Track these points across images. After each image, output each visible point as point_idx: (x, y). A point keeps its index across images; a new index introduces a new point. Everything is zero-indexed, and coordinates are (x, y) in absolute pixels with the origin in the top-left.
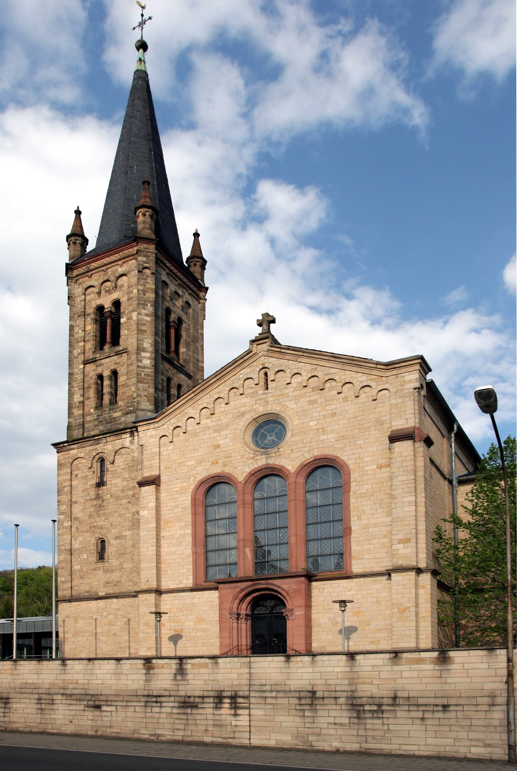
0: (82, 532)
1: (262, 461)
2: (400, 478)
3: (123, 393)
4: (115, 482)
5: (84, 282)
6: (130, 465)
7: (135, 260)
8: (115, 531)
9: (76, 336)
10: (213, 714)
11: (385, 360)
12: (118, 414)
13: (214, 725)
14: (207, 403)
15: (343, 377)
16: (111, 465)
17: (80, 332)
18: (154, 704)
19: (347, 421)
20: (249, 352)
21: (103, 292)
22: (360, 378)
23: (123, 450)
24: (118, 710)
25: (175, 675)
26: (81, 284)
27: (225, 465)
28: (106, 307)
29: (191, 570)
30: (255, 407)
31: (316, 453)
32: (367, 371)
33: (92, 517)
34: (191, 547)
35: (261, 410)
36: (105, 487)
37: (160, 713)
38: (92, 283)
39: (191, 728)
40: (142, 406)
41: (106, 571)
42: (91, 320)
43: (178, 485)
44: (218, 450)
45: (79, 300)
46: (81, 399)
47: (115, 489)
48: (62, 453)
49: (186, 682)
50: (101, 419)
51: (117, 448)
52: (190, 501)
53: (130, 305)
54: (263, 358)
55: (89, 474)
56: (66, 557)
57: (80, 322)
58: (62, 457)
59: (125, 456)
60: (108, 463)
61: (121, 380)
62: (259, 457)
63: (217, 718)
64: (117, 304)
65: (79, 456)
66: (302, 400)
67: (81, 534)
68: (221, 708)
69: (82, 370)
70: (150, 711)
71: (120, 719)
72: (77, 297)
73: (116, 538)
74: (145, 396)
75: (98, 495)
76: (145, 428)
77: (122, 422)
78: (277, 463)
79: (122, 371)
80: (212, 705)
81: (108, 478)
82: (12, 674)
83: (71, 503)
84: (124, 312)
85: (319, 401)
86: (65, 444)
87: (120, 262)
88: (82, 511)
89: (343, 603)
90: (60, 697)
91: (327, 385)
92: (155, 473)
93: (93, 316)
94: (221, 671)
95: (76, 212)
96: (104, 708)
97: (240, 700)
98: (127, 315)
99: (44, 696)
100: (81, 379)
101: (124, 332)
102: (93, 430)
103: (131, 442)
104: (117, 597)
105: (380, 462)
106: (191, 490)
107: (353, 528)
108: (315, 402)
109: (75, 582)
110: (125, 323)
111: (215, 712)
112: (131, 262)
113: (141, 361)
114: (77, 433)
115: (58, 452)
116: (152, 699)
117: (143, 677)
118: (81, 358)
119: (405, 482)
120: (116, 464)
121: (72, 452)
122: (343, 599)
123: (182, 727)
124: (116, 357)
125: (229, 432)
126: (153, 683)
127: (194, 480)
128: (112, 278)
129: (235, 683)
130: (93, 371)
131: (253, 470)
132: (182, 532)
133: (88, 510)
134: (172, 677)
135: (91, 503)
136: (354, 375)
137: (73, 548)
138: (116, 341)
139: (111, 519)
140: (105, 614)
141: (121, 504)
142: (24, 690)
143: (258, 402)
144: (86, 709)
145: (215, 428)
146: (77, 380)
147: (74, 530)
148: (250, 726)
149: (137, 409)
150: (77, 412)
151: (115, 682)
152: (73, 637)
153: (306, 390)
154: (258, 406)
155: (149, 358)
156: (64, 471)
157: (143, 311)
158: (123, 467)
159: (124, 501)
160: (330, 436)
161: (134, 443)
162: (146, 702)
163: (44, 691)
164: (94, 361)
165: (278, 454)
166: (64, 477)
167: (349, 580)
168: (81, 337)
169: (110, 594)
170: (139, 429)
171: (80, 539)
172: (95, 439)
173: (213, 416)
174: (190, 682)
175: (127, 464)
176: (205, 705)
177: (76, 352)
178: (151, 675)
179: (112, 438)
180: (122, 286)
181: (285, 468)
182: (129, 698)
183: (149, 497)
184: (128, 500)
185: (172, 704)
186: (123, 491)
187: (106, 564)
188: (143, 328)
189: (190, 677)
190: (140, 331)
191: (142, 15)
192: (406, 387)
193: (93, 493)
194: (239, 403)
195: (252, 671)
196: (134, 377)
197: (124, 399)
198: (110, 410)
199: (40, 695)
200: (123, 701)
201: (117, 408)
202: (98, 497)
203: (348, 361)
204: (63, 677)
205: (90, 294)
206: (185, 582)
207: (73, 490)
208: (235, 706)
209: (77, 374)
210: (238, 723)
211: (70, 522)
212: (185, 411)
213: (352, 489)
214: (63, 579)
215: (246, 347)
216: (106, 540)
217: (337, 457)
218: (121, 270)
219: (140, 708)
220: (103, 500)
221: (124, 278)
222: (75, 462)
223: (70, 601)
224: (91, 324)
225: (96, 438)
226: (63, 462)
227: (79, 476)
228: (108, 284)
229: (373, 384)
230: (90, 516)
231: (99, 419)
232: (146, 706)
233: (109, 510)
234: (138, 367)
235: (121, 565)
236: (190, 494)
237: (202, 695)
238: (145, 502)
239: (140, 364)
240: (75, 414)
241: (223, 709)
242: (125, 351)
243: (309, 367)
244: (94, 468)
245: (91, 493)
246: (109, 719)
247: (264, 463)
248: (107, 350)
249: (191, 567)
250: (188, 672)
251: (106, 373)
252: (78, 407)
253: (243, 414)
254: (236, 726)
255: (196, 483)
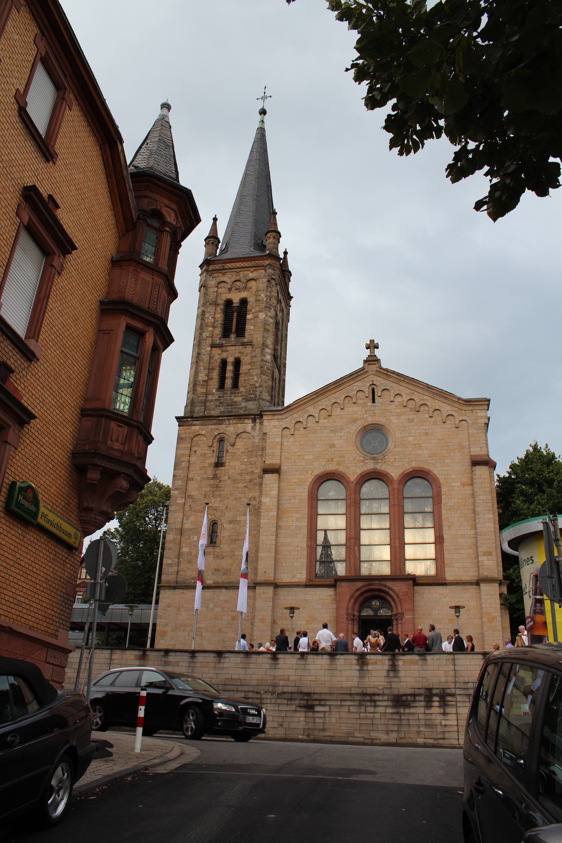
0: (195, 511)
1: (370, 466)
2: (481, 497)
3: (245, 380)
4: (234, 465)
5: (218, 277)
6: (250, 449)
7: (264, 271)
8: (229, 515)
9: (206, 321)
10: (425, 713)
11: (465, 397)
12: (239, 399)
13: (426, 725)
14: (326, 405)
15: (434, 405)
16: (231, 447)
17: (210, 318)
18: (368, 704)
19: (437, 441)
20: (362, 369)
21: (233, 289)
22: (446, 408)
23: (244, 434)
24: (332, 710)
25: (388, 671)
26: (215, 277)
27: (339, 464)
28: (234, 302)
29: (305, 565)
30: (365, 416)
31: (414, 465)
32: (451, 403)
33: (207, 496)
34: (305, 540)
35: (370, 420)
36: (223, 468)
37: (374, 713)
38: (225, 279)
39: (404, 729)
40: (263, 397)
41: (216, 557)
42: (221, 309)
43: (297, 477)
44: (333, 449)
45: (212, 291)
46: (206, 378)
47: (233, 471)
48: (184, 427)
49: (398, 680)
50: (222, 401)
51: (239, 432)
52: (307, 494)
53: (257, 306)
54: (372, 376)
55: (209, 452)
56: (175, 536)
57: (211, 309)
58: (183, 431)
59: (245, 440)
60: (228, 444)
61: (244, 368)
62: (368, 461)
63: (428, 717)
64: (244, 302)
65: (200, 432)
66: (402, 417)
67: (194, 513)
68: (431, 707)
69: (209, 352)
70: (363, 711)
71: (334, 720)
72: (210, 287)
73: (230, 522)
74: (266, 387)
75: (215, 475)
76: (270, 417)
77: (243, 408)
78: (383, 469)
79: (245, 360)
80: (423, 704)
81: (227, 459)
82: (215, 668)
83: (188, 479)
84: (251, 310)
85: (416, 420)
86: (189, 419)
87: (252, 269)
88: (198, 489)
89: (457, 608)
90: (269, 696)
91: (422, 409)
92: (276, 461)
93: (222, 307)
94: (430, 668)
95: (213, 219)
96: (317, 708)
97: (449, 698)
98: (253, 313)
99: (251, 695)
100: (207, 360)
101: (249, 327)
102: (214, 410)
103: (253, 428)
104: (226, 588)
105: (463, 480)
106: (308, 483)
107: (445, 537)
108: (413, 420)
109: (182, 566)
110: (251, 319)
111: (427, 712)
112: (260, 271)
113: (265, 356)
114: (199, 411)
115: (179, 426)
116: (368, 698)
117: (357, 674)
118: (209, 341)
119: (485, 501)
120: (236, 447)
121: (193, 428)
122: (292, 606)
123: (395, 728)
124: (240, 347)
125: (343, 434)
126: (367, 680)
127: (311, 474)
128: (243, 280)
129: (443, 680)
130: (218, 355)
131: (364, 472)
132: (298, 524)
133: (204, 489)
134: (384, 673)
135: (208, 482)
136: (441, 404)
137: (183, 527)
138: (241, 332)
139: (226, 501)
140: (211, 606)
141: (238, 488)
142: (228, 687)
143: (368, 412)
144: (298, 709)
145: (331, 429)
146: (203, 360)
147: (187, 508)
148: (457, 725)
149: (260, 399)
150: (200, 390)
151: (328, 678)
152: (173, 631)
153: (405, 409)
154: (367, 415)
155: (270, 354)
156: (183, 446)
157: (269, 314)
158: (242, 451)
159: (241, 485)
160: (425, 452)
161: (255, 429)
162: (360, 700)
163: (251, 689)
164: (220, 346)
165: (383, 461)
166: (182, 452)
167: (444, 587)
168: (211, 323)
169: (218, 583)
170: (265, 418)
171: (192, 518)
172: (218, 419)
173: (330, 417)
174: (402, 679)
175: (247, 449)
176: (417, 704)
177: (205, 335)
178: (365, 672)
179: (234, 421)
180: (251, 288)
181: (389, 474)
182: (344, 697)
183: (272, 485)
184: (245, 484)
185: (385, 703)
186: (240, 474)
187: (217, 550)
188: (268, 327)
189: (402, 674)
190: (266, 330)
191: (265, 93)
192: (479, 421)
193: (210, 472)
194: (351, 409)
195: (456, 669)
196: (258, 368)
197: (246, 386)
198: (231, 393)
199: (247, 693)
200: (336, 700)
201: (238, 393)
202: (215, 477)
203: (438, 393)
204: (272, 672)
205: (221, 288)
206: (298, 576)
207: (190, 466)
208: (444, 703)
209: (204, 355)
210: (447, 723)
211: (184, 499)
212: (307, 409)
213: (443, 501)
214: (169, 561)
215: (361, 365)
216: (219, 523)
217: (430, 471)
218: (251, 275)
219: (355, 707)
220: (220, 481)
221: (253, 282)
222: (195, 438)
223: (175, 588)
224: (220, 313)
225: (220, 418)
226: (183, 436)
227: (198, 452)
228: (238, 283)
229: (455, 414)
230: (205, 495)
231: (221, 400)
232: (360, 705)
233: (225, 492)
234: (262, 360)
235: (233, 552)
236: (307, 487)
237: (413, 693)
238: (268, 489)
239: (264, 358)
240: (198, 391)
241: (433, 708)
242: (250, 344)
243: (408, 391)
244: (214, 447)
245: (208, 471)
246: (321, 721)
247: (372, 467)
248: (232, 339)
249: (305, 560)
250: (400, 669)
251: (231, 360)
252: (202, 385)
253: (355, 420)
254: (446, 726)
255: (313, 477)
